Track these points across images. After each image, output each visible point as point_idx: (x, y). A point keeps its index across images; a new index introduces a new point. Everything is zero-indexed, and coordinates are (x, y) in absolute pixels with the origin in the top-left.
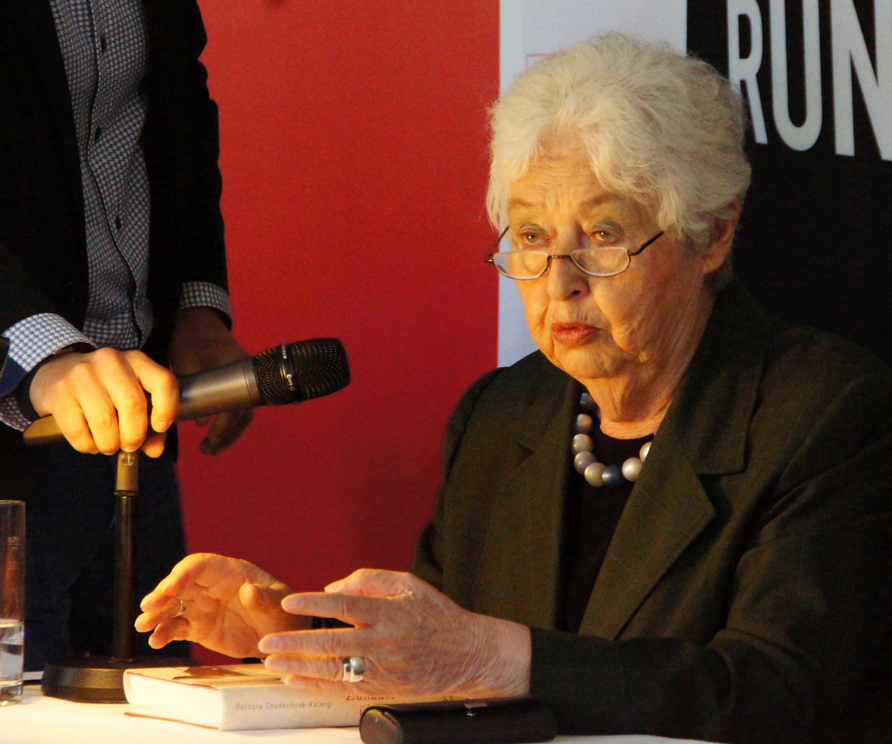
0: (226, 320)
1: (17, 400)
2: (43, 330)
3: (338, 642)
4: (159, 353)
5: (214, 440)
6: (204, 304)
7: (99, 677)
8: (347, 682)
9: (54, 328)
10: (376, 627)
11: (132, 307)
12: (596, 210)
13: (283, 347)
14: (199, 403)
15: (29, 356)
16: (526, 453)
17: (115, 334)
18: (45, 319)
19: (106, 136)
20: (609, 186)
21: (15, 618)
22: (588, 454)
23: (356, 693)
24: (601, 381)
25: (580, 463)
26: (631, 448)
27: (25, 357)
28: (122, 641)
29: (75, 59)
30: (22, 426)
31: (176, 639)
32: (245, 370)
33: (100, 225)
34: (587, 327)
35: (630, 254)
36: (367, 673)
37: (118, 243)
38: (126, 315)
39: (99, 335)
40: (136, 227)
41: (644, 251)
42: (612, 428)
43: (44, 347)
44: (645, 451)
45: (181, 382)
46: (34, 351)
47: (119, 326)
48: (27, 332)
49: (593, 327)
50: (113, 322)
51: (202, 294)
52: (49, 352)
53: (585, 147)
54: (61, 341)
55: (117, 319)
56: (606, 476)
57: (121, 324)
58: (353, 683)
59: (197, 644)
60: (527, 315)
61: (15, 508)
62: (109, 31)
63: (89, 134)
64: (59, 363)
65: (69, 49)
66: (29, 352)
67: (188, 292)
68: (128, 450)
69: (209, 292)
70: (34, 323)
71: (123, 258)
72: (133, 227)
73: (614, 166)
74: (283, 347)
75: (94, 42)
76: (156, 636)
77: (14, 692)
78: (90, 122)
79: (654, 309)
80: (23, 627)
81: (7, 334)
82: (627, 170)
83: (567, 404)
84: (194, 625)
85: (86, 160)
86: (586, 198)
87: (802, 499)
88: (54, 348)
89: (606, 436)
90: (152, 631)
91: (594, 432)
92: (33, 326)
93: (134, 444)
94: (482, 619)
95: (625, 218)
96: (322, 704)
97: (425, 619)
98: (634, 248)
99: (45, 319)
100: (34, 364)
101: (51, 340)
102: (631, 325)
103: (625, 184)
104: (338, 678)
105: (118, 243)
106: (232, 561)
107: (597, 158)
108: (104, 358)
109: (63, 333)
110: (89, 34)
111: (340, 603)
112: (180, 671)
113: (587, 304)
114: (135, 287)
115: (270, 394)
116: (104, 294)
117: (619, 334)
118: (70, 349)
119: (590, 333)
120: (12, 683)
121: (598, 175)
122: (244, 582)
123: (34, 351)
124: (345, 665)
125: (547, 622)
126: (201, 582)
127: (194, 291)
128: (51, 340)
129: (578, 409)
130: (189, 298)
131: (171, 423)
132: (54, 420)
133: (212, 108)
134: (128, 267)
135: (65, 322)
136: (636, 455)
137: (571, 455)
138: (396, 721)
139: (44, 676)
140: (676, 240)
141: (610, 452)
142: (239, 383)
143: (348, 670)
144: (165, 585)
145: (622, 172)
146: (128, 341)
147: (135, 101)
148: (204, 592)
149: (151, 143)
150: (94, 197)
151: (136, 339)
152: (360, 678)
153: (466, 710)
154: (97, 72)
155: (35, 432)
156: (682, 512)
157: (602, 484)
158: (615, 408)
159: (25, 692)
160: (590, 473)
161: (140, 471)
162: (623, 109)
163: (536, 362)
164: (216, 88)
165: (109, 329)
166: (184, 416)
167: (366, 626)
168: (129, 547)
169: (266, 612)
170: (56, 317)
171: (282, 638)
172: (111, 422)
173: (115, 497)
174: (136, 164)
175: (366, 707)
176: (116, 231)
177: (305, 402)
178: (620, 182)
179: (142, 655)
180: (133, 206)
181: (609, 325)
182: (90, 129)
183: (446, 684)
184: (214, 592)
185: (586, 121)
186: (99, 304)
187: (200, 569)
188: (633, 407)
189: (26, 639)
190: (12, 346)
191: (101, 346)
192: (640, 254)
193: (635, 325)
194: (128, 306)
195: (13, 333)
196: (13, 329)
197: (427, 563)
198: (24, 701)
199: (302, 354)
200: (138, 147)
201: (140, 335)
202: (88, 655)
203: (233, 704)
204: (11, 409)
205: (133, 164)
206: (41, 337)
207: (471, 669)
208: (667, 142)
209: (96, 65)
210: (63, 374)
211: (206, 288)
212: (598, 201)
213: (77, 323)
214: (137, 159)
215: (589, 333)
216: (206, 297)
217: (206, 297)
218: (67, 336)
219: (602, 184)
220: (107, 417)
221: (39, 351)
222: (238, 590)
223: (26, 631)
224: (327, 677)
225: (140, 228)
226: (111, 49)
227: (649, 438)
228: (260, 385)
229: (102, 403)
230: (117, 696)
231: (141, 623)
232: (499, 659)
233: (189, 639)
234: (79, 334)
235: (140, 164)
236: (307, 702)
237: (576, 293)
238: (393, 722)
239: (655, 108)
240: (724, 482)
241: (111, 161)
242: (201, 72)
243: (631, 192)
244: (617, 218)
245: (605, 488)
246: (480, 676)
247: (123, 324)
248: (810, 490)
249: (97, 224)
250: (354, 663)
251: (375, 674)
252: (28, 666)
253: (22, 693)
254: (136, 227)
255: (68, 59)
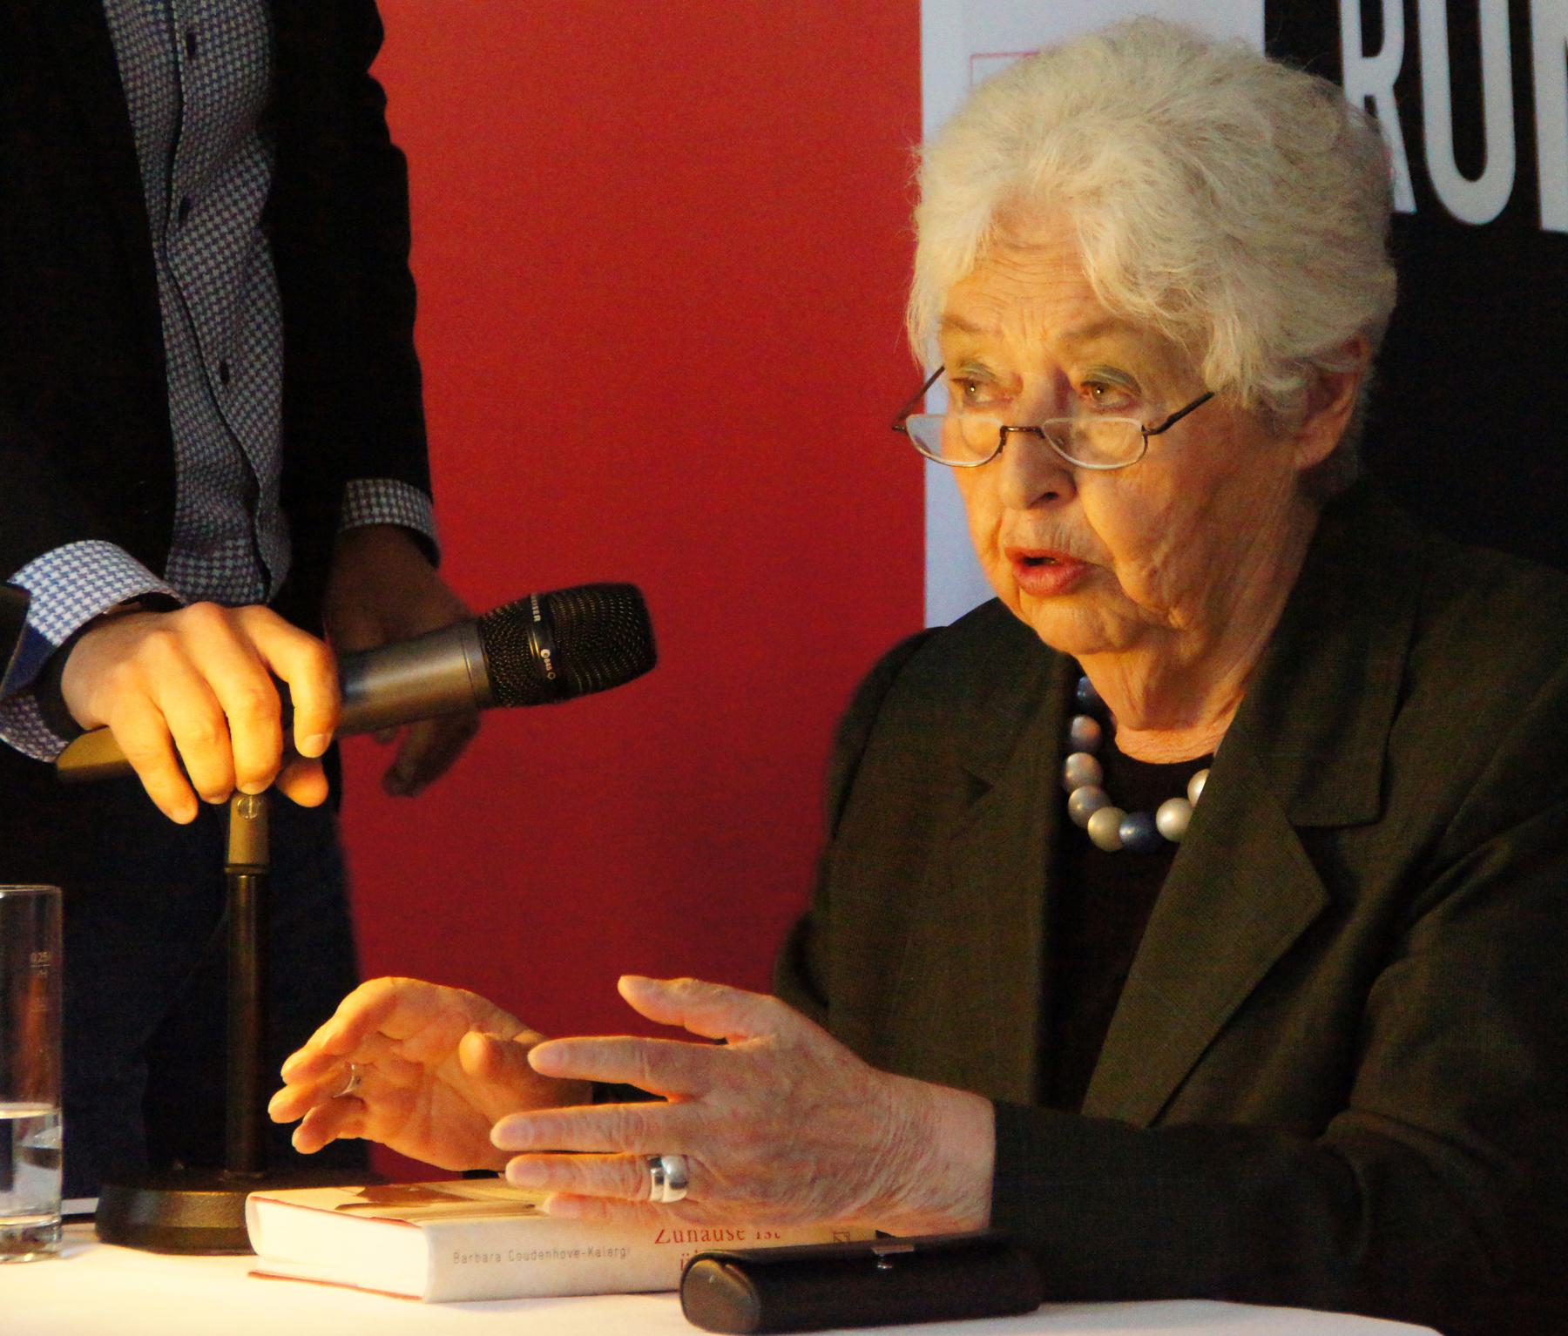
0: (425, 547)
1: (38, 699)
2: (84, 571)
3: (639, 1128)
4: (300, 611)
5: (407, 770)
6: (388, 520)
7: (201, 1207)
8: (658, 1202)
9: (105, 567)
10: (707, 1099)
11: (252, 526)
12: (1089, 348)
13: (534, 601)
14: (379, 702)
15: (59, 617)
16: (979, 788)
17: (221, 577)
18: (89, 550)
19: (199, 214)
20: (1116, 304)
21: (44, 1101)
22: (1094, 791)
23: (675, 1222)
24: (1108, 657)
25: (1079, 807)
26: (1171, 780)
27: (51, 619)
28: (242, 1146)
29: (138, 72)
30: (46, 752)
31: (342, 1135)
32: (463, 642)
33: (191, 378)
34: (1074, 561)
35: (1146, 433)
36: (694, 1183)
37: (227, 410)
38: (241, 542)
39: (191, 580)
40: (258, 380)
41: (1176, 427)
42: (1135, 743)
43: (87, 601)
44: (1198, 786)
45: (344, 665)
46: (68, 609)
47: (229, 563)
48: (55, 575)
49: (1081, 562)
50: (217, 554)
51: (383, 500)
52: (95, 609)
53: (1075, 230)
54: (118, 590)
55: (224, 549)
56: (1126, 832)
57: (231, 560)
58: (669, 1204)
59: (383, 1146)
60: (969, 537)
61: (42, 898)
62: (202, 21)
63: (168, 210)
64: (114, 632)
65: (128, 53)
66: (60, 610)
67: (357, 498)
68: (249, 789)
69: (396, 496)
70: (68, 557)
71: (234, 438)
72: (252, 381)
73: (1126, 269)
74: (534, 601)
75: (173, 40)
76: (306, 1131)
77: (45, 1237)
78: (169, 189)
79: (1200, 521)
80: (60, 1117)
81: (19, 578)
82: (1150, 275)
83: (1053, 699)
84: (376, 1108)
85: (164, 258)
86: (1075, 325)
87: (1487, 871)
88: (105, 602)
89: (1125, 757)
90: (298, 1123)
91: (1104, 749)
92: (67, 563)
93: (260, 779)
94: (907, 1084)
95: (1150, 366)
96: (610, 1252)
97: (797, 1085)
98: (1158, 419)
99: (89, 550)
100: (67, 632)
101: (98, 589)
102: (1150, 559)
103: (1142, 303)
104: (639, 1197)
105: (227, 410)
106: (445, 993)
107: (1096, 253)
108: (199, 622)
109: (121, 575)
110: (163, 27)
111: (637, 1054)
112: (350, 1194)
113: (1070, 516)
114: (258, 489)
115: (510, 684)
116: (203, 506)
117: (1129, 576)
118: (136, 605)
119: (1079, 574)
120: (42, 1221)
121: (1095, 287)
122: (467, 1031)
123: (68, 609)
124: (654, 1171)
125: (1022, 1092)
126: (387, 1030)
127: (368, 496)
128: (98, 589)
129: (1074, 707)
130: (359, 508)
131: (329, 736)
132: (111, 735)
133: (393, 165)
134: (244, 454)
135: (126, 557)
136: (1183, 793)
137: (1063, 794)
138: (745, 1279)
139: (100, 1206)
140: (1238, 407)
141: (1135, 787)
142: (454, 666)
143: (660, 1180)
144: (325, 1035)
145: (1141, 280)
146: (246, 590)
147: (252, 148)
148: (395, 1050)
149: (281, 222)
150: (180, 326)
151: (261, 586)
152: (682, 1194)
153: (876, 1258)
154: (181, 95)
155: (77, 757)
156: (1271, 894)
157: (1118, 846)
158: (1133, 707)
159: (66, 1237)
160: (1097, 825)
161: (270, 821)
162: (1148, 162)
163: (993, 621)
164: (404, 123)
165: (210, 568)
166: (350, 724)
167: (688, 1098)
168: (253, 968)
169: (508, 1084)
170: (109, 546)
171: (534, 1120)
172: (217, 739)
173: (225, 875)
174: (257, 264)
175: (692, 1255)
176: (220, 388)
177: (574, 700)
178: (1135, 299)
179: (280, 1166)
180: (252, 341)
181: (1111, 559)
182: (169, 199)
183: (839, 1204)
184: (413, 1050)
185: (1082, 180)
186: (191, 522)
187: (388, 1005)
188: (1170, 700)
189: (65, 1139)
190: (35, 606)
191: (193, 599)
192: (1164, 434)
193: (1157, 559)
194: (244, 525)
195: (29, 577)
196: (29, 569)
197: (803, 986)
198: (64, 1253)
199: (580, 614)
200: (260, 233)
201: (267, 578)
202: (180, 1166)
203: (448, 1253)
204: (28, 719)
205: (250, 263)
206: (73, 576)
207: (884, 1176)
208: (1225, 227)
209: (178, 82)
210: (126, 651)
211: (391, 491)
212: (1095, 331)
213: (153, 561)
214: (258, 256)
215: (1075, 575)
216: (390, 506)
217: (390, 506)
218: (129, 581)
219: (1104, 303)
220: (209, 728)
221: (77, 608)
222: (457, 1043)
223: (66, 1123)
224: (621, 1195)
225: (265, 381)
226: (205, 54)
227: (1203, 762)
228: (492, 667)
229: (196, 705)
230: (235, 1242)
231: (279, 1106)
232: (937, 1159)
233: (365, 1136)
234: (150, 577)
235: (264, 264)
236: (583, 1248)
237: (1050, 496)
238: (743, 1284)
239: (1210, 163)
240: (1345, 839)
241: (211, 253)
242: (376, 94)
243: (1154, 317)
244: (1127, 366)
245: (1125, 852)
246: (900, 1188)
247: (235, 557)
248: (1501, 852)
249: (186, 375)
250: (669, 1167)
251: (708, 1187)
252: (71, 1189)
253: (60, 1236)
254: (258, 380)
255: (134, 101)
